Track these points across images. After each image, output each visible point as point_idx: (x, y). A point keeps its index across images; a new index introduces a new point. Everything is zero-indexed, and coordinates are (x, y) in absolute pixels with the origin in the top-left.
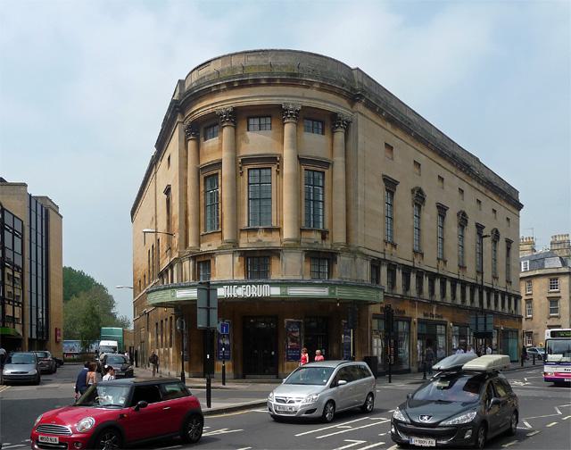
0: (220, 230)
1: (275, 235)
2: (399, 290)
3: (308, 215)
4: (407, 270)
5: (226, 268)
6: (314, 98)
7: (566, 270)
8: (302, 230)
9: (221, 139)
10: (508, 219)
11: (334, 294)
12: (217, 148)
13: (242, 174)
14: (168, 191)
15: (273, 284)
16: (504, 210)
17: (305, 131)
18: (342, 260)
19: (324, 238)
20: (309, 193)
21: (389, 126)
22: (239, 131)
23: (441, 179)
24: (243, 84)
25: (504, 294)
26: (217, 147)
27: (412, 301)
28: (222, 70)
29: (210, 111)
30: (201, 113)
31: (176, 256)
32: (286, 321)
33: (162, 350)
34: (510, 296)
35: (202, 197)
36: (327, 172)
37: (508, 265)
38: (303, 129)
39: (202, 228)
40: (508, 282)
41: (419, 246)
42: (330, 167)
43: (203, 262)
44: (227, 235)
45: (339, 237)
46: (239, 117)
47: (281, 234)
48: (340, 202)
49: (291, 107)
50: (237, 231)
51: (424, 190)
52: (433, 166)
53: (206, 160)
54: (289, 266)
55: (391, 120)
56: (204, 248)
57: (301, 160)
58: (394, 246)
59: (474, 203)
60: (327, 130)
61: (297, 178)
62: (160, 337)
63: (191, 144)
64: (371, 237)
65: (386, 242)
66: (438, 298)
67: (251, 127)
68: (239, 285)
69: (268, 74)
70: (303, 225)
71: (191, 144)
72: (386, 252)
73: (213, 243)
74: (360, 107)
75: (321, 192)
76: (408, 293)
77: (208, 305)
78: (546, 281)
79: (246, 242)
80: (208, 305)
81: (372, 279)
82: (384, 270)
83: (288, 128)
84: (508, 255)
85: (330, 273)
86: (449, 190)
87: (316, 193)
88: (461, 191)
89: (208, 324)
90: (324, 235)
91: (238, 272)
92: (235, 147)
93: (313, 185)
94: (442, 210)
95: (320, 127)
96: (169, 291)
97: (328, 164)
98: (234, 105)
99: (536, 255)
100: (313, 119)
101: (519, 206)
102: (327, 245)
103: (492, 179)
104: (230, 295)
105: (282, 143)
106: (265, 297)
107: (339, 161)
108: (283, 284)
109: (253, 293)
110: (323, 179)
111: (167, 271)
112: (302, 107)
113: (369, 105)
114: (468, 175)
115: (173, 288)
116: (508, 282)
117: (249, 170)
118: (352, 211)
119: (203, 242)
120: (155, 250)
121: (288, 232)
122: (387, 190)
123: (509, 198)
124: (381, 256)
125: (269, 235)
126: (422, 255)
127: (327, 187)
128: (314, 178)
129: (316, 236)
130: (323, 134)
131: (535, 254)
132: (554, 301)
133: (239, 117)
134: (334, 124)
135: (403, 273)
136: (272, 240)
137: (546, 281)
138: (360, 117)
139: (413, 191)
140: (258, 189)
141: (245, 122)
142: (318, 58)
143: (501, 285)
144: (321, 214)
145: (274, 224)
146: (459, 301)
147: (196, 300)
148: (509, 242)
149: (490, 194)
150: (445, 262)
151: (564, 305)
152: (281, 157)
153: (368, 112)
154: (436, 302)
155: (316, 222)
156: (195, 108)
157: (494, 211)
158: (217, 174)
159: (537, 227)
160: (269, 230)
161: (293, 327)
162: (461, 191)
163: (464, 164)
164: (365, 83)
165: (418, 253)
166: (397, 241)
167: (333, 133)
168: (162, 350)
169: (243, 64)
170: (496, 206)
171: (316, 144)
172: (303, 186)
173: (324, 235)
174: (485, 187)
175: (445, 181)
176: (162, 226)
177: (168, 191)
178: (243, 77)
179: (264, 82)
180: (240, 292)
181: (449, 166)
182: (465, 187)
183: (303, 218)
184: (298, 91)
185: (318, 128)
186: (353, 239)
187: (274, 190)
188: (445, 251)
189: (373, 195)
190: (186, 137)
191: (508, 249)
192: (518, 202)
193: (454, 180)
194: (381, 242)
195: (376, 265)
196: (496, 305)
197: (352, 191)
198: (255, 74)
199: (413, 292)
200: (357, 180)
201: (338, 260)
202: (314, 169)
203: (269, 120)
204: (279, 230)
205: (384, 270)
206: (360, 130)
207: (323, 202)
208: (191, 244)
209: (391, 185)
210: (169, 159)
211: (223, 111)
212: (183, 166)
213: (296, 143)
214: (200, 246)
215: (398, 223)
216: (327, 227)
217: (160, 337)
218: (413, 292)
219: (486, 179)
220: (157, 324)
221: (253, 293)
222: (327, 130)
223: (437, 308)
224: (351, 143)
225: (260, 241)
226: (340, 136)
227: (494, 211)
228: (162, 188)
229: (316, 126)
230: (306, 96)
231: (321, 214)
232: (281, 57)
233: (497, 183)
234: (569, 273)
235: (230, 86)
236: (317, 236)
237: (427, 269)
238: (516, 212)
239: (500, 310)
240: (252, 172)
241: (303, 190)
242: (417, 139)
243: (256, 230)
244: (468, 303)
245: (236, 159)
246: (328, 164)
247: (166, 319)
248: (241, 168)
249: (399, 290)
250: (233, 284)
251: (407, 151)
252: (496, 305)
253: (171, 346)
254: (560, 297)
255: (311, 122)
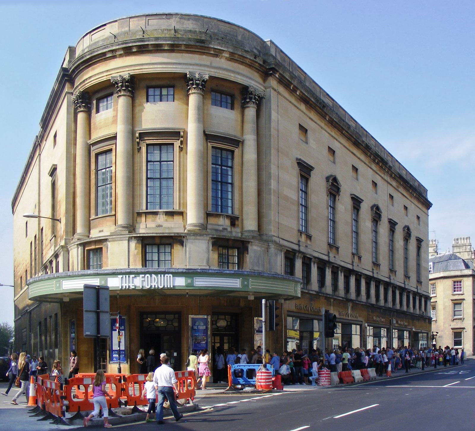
0: (113, 213)
1: (178, 219)
2: (315, 285)
3: (215, 198)
4: (323, 265)
5: (120, 254)
6: (221, 67)
7: (469, 272)
8: (208, 215)
9: (116, 110)
10: (418, 218)
11: (248, 286)
12: (111, 120)
13: (139, 149)
14: (53, 171)
15: (176, 274)
16: (414, 207)
17: (212, 105)
18: (254, 249)
19: (233, 224)
20: (217, 173)
21: (303, 107)
22: (137, 101)
23: (355, 169)
24: (143, 50)
25: (415, 294)
26: (111, 118)
27: (327, 298)
28: (120, 34)
29: (105, 79)
30: (94, 81)
31: (63, 243)
32: (191, 316)
33: (46, 352)
34: (421, 296)
35: (93, 176)
36: (237, 152)
37: (418, 265)
38: (210, 102)
39: (93, 211)
40: (419, 282)
41: (334, 240)
42: (240, 145)
43: (93, 251)
44: (121, 219)
45: (250, 224)
46: (137, 87)
47: (185, 219)
48: (250, 185)
49: (197, 76)
50: (134, 215)
51: (339, 178)
52: (348, 155)
53: (96, 135)
54: (195, 254)
55: (304, 100)
56: (95, 234)
57: (208, 137)
58: (309, 237)
59: (387, 198)
60: (237, 105)
61: (202, 157)
62: (43, 338)
63: (81, 117)
64: (285, 225)
65: (301, 233)
66: (353, 295)
67: (151, 98)
68: (137, 274)
69: (170, 39)
70: (210, 209)
71: (81, 117)
72: (301, 244)
73: (105, 229)
74: (273, 82)
75: (230, 173)
76: (323, 290)
77: (98, 307)
78: (449, 283)
79: (147, 227)
80: (98, 307)
81: (286, 272)
82: (299, 264)
83: (193, 99)
84: (418, 254)
85: (240, 264)
86: (362, 182)
87: (224, 174)
88: (375, 184)
89: (98, 331)
90: (234, 221)
91: (135, 261)
92: (132, 118)
93: (222, 165)
94: (357, 202)
95: (229, 101)
96: (54, 281)
97: (237, 143)
98: (132, 73)
99: (440, 257)
100: (219, 91)
101: (428, 205)
102: (236, 233)
103: (403, 173)
104: (125, 285)
105: (185, 114)
106: (168, 289)
107: (250, 140)
108: (189, 273)
109: (153, 284)
110: (233, 159)
111: (51, 262)
112: (210, 77)
113: (282, 81)
114: (381, 167)
115: (58, 277)
116: (419, 282)
117: (148, 145)
118: (264, 195)
119: (95, 227)
120: (39, 239)
121: (193, 217)
122: (301, 175)
123: (418, 194)
124: (296, 247)
125: (170, 219)
126: (337, 249)
127: (237, 167)
128: (221, 157)
129: (223, 222)
130: (232, 108)
131: (439, 256)
132: (457, 303)
133: (137, 87)
134: (246, 99)
135: (318, 268)
136: (173, 226)
137: (449, 283)
138: (273, 94)
139: (328, 179)
140: (158, 167)
141: (145, 91)
142: (228, 25)
143: (412, 285)
144: (230, 197)
145: (176, 208)
146: (373, 300)
147: (81, 293)
148: (419, 241)
149: (401, 189)
150: (360, 258)
151: (467, 308)
152: (186, 133)
153: (281, 89)
154: (352, 301)
155: (224, 207)
156: (85, 78)
157: (406, 208)
158: (110, 150)
159: (446, 229)
160: (171, 214)
161: (199, 321)
162: (375, 184)
163: (379, 156)
164: (278, 58)
165: (333, 246)
166: (312, 232)
167: (243, 108)
168: (46, 352)
169: (144, 28)
170: (408, 203)
171: (225, 119)
172: (210, 166)
173: (234, 221)
174: (397, 181)
175: (359, 171)
176: (46, 211)
177: (53, 171)
178: (142, 41)
179: (166, 48)
180: (138, 283)
181: (362, 157)
182: (378, 180)
183: (210, 202)
184: (205, 60)
185: (227, 103)
186: (265, 226)
187: (177, 169)
188: (361, 249)
189: (285, 179)
190: (75, 110)
191: (419, 248)
192: (427, 200)
193: (368, 172)
194: (296, 232)
195: (290, 257)
196: (408, 305)
197: (264, 174)
198: (157, 39)
199: (328, 289)
200: (270, 162)
201: (249, 250)
202: (221, 149)
203: (171, 91)
204: (181, 214)
205: (299, 264)
206: (273, 106)
207: (232, 184)
208: (79, 229)
209: (305, 170)
210: (55, 136)
211: (119, 79)
212: (72, 142)
213: (203, 117)
214: (89, 232)
215: (313, 213)
216: (237, 213)
217: (43, 338)
218: (328, 289)
219: (399, 174)
220: (26, 271)
221: (153, 284)
222: (237, 105)
223: (352, 307)
224: (263, 120)
225: (159, 226)
226: (251, 112)
227: (406, 208)
228: (46, 169)
229: (224, 100)
230: (214, 65)
231: (230, 197)
232: (186, 22)
233: (408, 178)
234: (472, 275)
235: (128, 51)
236: (227, 222)
237: (343, 264)
238: (424, 209)
239: (412, 310)
240: (151, 148)
241: (210, 170)
242: (332, 124)
243: (155, 213)
244: (382, 303)
245: (133, 132)
246: (237, 143)
247: (51, 317)
248: (138, 143)
249: (315, 285)
250: (130, 273)
251: (322, 136)
252: (408, 305)
253: (56, 347)
254: (464, 300)
255: (219, 95)
